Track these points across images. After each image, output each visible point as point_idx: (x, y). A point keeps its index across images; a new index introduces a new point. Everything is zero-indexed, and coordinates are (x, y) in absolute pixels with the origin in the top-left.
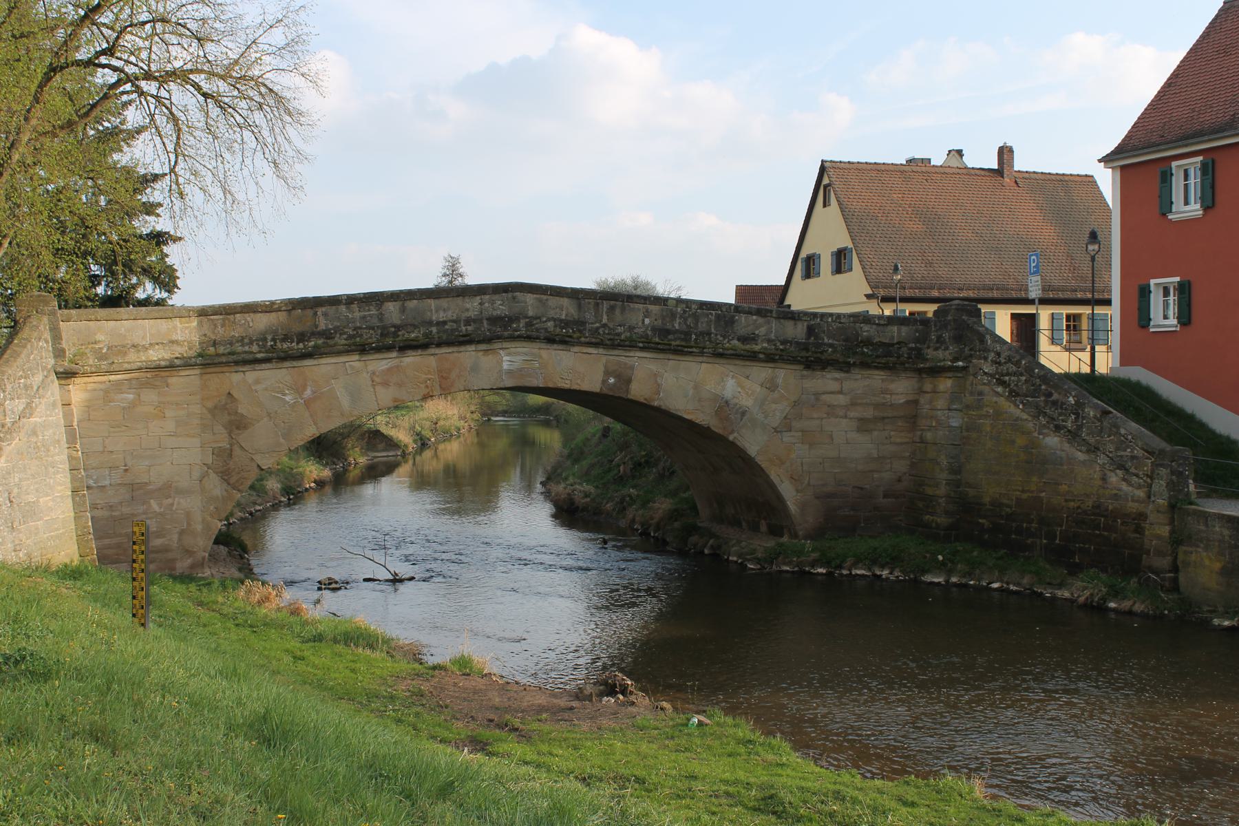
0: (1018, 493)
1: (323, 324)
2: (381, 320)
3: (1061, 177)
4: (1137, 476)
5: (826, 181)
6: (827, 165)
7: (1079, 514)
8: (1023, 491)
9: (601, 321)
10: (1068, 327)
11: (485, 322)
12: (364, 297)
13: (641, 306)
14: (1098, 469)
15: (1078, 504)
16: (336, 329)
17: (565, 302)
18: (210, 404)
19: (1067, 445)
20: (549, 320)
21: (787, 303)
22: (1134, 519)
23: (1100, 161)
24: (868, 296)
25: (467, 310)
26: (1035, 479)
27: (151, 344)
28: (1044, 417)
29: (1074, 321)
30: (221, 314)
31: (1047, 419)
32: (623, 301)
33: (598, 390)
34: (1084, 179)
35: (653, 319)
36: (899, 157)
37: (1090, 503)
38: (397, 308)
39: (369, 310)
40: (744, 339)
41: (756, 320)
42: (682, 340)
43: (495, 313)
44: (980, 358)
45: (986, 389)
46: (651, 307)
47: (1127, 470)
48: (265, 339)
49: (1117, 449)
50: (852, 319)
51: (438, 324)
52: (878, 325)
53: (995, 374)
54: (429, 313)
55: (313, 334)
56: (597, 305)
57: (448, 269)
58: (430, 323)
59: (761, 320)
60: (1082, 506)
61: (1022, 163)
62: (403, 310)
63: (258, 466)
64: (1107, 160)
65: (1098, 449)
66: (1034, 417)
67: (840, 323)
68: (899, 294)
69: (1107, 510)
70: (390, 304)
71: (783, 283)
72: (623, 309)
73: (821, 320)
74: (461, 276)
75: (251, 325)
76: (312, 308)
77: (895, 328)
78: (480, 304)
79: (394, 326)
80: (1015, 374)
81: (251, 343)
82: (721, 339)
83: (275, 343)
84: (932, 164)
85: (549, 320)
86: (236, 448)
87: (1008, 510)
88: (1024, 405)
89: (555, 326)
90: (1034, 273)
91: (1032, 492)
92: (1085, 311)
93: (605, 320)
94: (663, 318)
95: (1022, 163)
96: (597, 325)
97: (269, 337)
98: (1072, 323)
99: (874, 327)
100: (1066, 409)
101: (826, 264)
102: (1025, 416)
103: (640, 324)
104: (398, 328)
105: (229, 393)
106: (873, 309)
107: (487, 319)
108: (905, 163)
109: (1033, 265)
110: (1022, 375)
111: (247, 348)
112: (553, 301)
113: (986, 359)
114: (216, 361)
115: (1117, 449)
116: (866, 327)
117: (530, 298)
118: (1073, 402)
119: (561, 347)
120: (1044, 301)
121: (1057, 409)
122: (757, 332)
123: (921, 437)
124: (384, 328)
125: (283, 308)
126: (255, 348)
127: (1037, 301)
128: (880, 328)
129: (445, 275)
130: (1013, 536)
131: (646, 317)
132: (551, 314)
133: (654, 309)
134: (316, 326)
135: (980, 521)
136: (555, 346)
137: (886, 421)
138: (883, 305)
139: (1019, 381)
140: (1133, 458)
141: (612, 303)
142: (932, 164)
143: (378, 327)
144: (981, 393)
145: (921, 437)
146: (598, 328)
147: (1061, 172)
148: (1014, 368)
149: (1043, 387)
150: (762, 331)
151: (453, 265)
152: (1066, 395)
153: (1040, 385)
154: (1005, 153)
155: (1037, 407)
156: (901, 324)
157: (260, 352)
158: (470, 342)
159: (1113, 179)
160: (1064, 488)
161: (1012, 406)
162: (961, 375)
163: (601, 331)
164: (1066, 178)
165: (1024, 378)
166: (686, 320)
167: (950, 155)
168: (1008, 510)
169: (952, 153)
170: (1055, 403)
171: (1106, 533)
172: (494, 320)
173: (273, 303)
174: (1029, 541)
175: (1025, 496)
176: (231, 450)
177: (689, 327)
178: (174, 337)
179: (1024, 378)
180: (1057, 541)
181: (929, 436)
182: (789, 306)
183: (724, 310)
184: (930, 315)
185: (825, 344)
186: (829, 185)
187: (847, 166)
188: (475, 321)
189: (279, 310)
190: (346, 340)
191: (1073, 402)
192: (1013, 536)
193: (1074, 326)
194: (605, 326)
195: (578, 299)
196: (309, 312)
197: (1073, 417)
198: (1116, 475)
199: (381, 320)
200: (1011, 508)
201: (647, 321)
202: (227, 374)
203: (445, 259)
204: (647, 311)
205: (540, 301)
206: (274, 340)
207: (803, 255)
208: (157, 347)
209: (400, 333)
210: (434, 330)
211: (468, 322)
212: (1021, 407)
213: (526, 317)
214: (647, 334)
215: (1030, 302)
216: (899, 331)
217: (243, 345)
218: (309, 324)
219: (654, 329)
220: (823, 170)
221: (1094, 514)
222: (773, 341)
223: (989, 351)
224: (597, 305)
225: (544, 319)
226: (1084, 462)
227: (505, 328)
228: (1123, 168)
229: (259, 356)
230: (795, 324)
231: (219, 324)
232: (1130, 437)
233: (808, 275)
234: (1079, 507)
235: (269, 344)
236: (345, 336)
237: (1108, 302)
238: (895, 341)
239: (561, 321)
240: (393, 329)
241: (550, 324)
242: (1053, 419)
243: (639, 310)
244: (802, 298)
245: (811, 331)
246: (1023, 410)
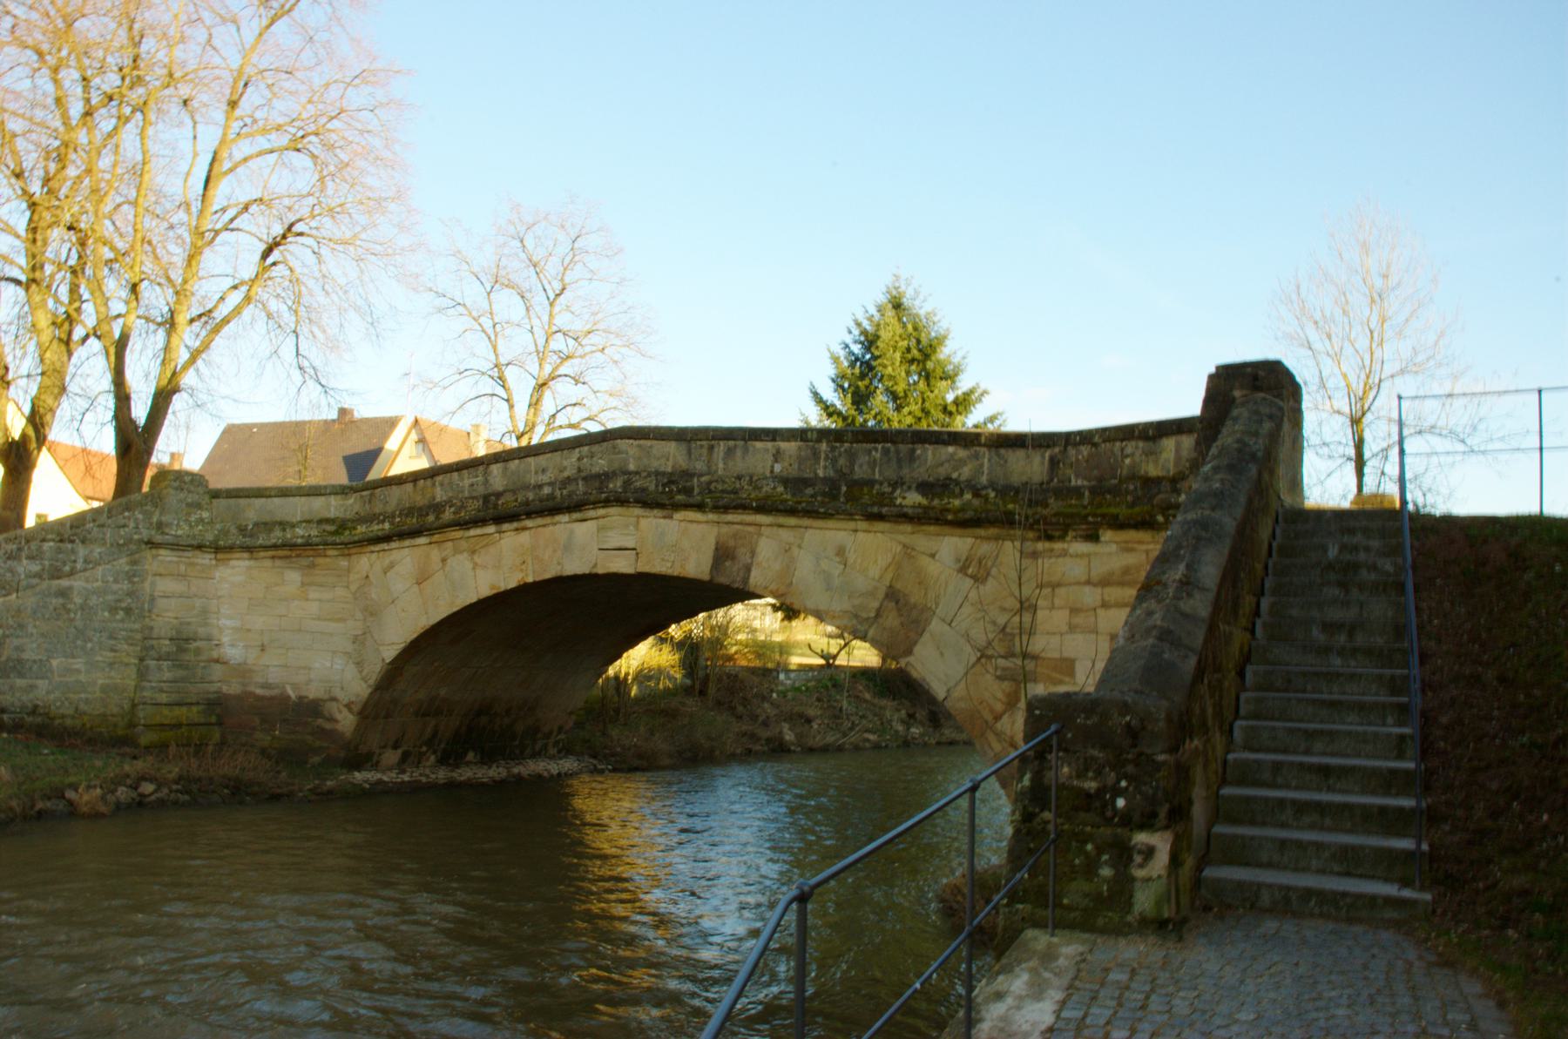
23: (985, 392)
33: (706, 577)
35: (786, 464)
141: (731, 443)
177: (839, 472)
224: (711, 448)
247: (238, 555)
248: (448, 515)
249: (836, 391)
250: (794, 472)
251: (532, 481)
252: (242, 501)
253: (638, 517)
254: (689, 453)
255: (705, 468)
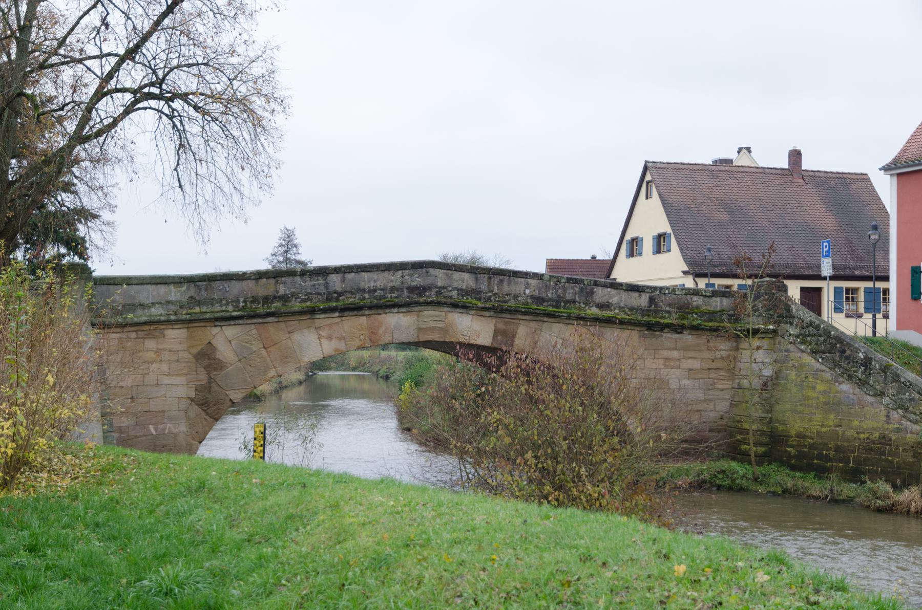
0: (818, 427)
1: (282, 290)
2: (327, 288)
3: (840, 175)
4: (915, 414)
5: (648, 177)
6: (649, 165)
7: (869, 443)
8: (822, 426)
9: (492, 291)
10: (847, 298)
11: (405, 291)
12: (314, 270)
13: (523, 280)
14: (883, 409)
15: (867, 435)
16: (293, 294)
17: (466, 276)
18: (195, 351)
19: (858, 390)
20: (454, 289)
21: (612, 276)
22: (912, 447)
23: (880, 169)
24: (685, 273)
25: (392, 281)
26: (832, 416)
27: (152, 303)
28: (839, 368)
29: (852, 294)
30: (205, 281)
31: (842, 370)
32: (509, 276)
33: (490, 345)
34: (860, 177)
35: (532, 290)
36: (706, 158)
37: (876, 435)
38: (339, 278)
39: (318, 280)
40: (601, 306)
41: (610, 292)
42: (553, 306)
43: (413, 284)
44: (787, 323)
45: (791, 347)
46: (531, 281)
47: (906, 410)
48: (238, 301)
49: (898, 393)
50: (684, 291)
51: (370, 291)
52: (706, 296)
53: (799, 336)
54: (363, 283)
55: (275, 297)
56: (490, 278)
57: (284, 240)
58: (364, 290)
59: (613, 292)
60: (871, 437)
61: (807, 164)
62: (343, 281)
63: (231, 400)
64: (886, 169)
65: (883, 393)
66: (831, 369)
67: (675, 294)
68: (709, 271)
69: (890, 440)
70: (333, 275)
71: (611, 258)
72: (509, 283)
73: (660, 292)
74: (296, 247)
75: (228, 289)
76: (274, 278)
77: (718, 299)
78: (402, 276)
79: (336, 292)
80: (815, 336)
81: (227, 304)
82: (584, 306)
83: (246, 304)
84: (734, 164)
85: (454, 289)
86: (213, 385)
87: (811, 441)
88: (823, 359)
89: (458, 295)
90: (826, 256)
91: (830, 426)
92: (862, 285)
93: (496, 290)
94: (540, 289)
95: (807, 164)
96: (490, 294)
97: (242, 300)
98: (850, 295)
99: (702, 298)
100: (857, 362)
101: (648, 245)
102: (824, 368)
103: (522, 293)
104: (340, 294)
105: (210, 343)
106: (689, 283)
107: (407, 289)
108: (711, 163)
109: (825, 250)
110: (821, 336)
111: (224, 308)
112: (457, 275)
113: (791, 324)
114: (201, 317)
115: (898, 393)
116: (695, 298)
117: (440, 273)
118: (862, 357)
119: (462, 311)
120: (833, 278)
121: (849, 362)
122: (610, 301)
123: (739, 384)
124: (329, 294)
125: (253, 277)
126: (230, 308)
127: (828, 278)
128: (706, 299)
129: (281, 245)
130: (815, 461)
131: (526, 288)
132: (455, 285)
133: (533, 282)
134: (277, 292)
135: (788, 449)
136: (458, 310)
137: (711, 371)
138: (698, 280)
139: (818, 340)
140: (911, 400)
141: (502, 277)
142: (734, 164)
143: (324, 293)
144: (787, 351)
145: (739, 384)
146: (490, 297)
147: (840, 171)
148: (815, 330)
149: (838, 345)
150: (615, 300)
151: (289, 237)
152: (856, 352)
153: (836, 344)
154: (795, 156)
155: (834, 361)
156: (723, 296)
157: (234, 311)
158: (395, 306)
159: (891, 183)
160: (856, 423)
161: (813, 360)
162: (771, 336)
163: (492, 299)
164: (845, 176)
165: (822, 339)
166: (557, 291)
167: (741, 153)
168: (811, 441)
169: (744, 150)
170: (847, 358)
171: (890, 458)
172: (412, 289)
173: (245, 274)
174: (829, 464)
175: (824, 430)
176: (210, 387)
177: (559, 296)
178: (170, 299)
179: (822, 339)
180: (851, 465)
181: (745, 383)
182: (615, 279)
183: (586, 283)
184: (735, 288)
185: (663, 311)
186: (651, 181)
187: (666, 166)
188: (397, 290)
189: (249, 278)
190: (300, 302)
191: (862, 357)
192: (815, 461)
193: (852, 297)
194: (495, 295)
195: (476, 273)
196: (272, 281)
197: (863, 368)
198: (898, 413)
199: (327, 288)
200: (813, 439)
201: (527, 292)
202: (209, 328)
203: (282, 231)
204: (527, 284)
205: (447, 275)
206: (245, 302)
207: (628, 237)
208: (157, 306)
209: (341, 298)
210: (367, 296)
211: (393, 290)
212: (820, 360)
213: (436, 287)
214: (528, 302)
215: (819, 277)
216: (721, 302)
217: (221, 306)
218: (272, 290)
219: (533, 298)
220: (646, 169)
221: (881, 443)
222: (623, 308)
223: (794, 317)
224: (490, 278)
225: (450, 289)
226: (872, 404)
227: (420, 295)
228: (899, 175)
229: (235, 314)
230: (640, 295)
231: (203, 288)
232: (908, 384)
233: (631, 254)
234: (868, 438)
235: (241, 305)
236: (299, 300)
237: (886, 279)
238: (718, 309)
239: (462, 290)
240: (336, 295)
241: (455, 293)
242: (846, 370)
243: (521, 282)
244: (625, 272)
245: (652, 300)
246: (822, 363)
247: (318, 316)
248: (296, 305)
249: (402, 433)
250: (536, 293)
251: (367, 287)
252: (111, 287)
253: (446, 312)
254: (477, 279)
255: (486, 288)
